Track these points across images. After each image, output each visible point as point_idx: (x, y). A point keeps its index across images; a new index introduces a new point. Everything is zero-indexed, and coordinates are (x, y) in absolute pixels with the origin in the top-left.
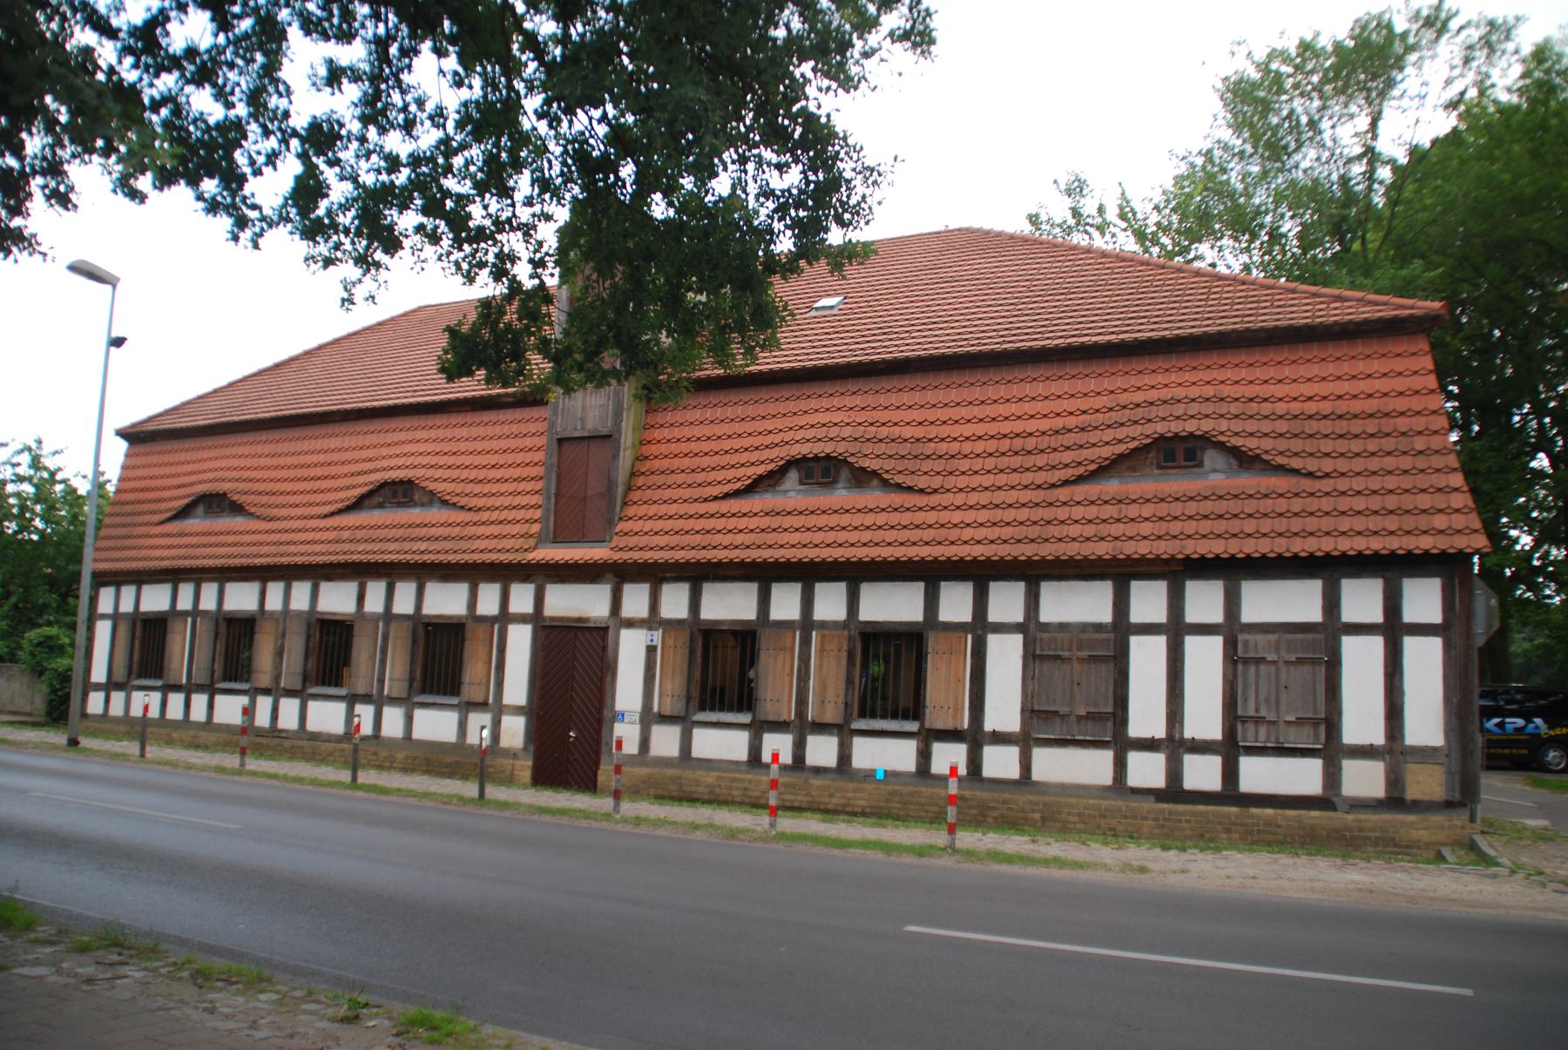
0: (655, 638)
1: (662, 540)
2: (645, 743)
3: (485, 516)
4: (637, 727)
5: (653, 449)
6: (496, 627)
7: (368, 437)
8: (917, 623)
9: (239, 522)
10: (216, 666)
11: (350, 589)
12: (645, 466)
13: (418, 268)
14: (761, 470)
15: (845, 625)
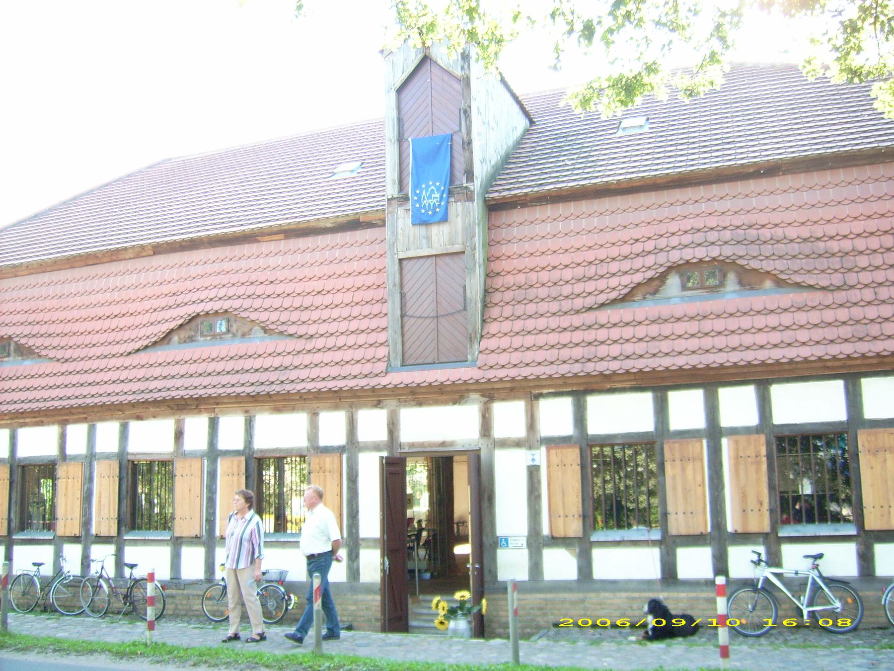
0: (537, 457)
1: (356, 369)
2: (536, 567)
3: (320, 343)
4: (526, 552)
5: (504, 265)
6: (345, 457)
7: (127, 277)
8: (841, 423)
9: (28, 365)
10: (12, 515)
11: (51, 432)
12: (498, 282)
13: (692, 8)
14: (638, 278)
15: (758, 430)
